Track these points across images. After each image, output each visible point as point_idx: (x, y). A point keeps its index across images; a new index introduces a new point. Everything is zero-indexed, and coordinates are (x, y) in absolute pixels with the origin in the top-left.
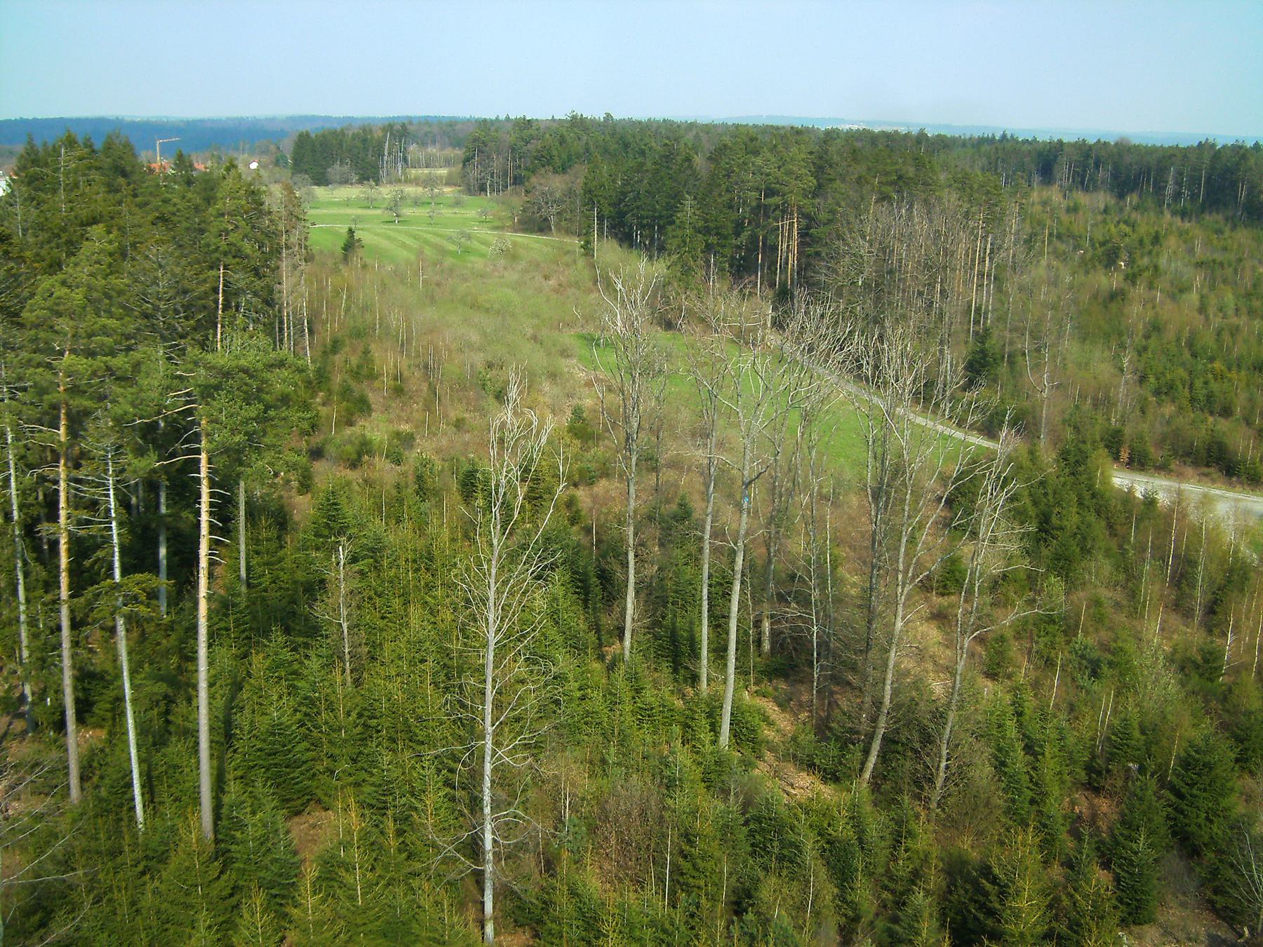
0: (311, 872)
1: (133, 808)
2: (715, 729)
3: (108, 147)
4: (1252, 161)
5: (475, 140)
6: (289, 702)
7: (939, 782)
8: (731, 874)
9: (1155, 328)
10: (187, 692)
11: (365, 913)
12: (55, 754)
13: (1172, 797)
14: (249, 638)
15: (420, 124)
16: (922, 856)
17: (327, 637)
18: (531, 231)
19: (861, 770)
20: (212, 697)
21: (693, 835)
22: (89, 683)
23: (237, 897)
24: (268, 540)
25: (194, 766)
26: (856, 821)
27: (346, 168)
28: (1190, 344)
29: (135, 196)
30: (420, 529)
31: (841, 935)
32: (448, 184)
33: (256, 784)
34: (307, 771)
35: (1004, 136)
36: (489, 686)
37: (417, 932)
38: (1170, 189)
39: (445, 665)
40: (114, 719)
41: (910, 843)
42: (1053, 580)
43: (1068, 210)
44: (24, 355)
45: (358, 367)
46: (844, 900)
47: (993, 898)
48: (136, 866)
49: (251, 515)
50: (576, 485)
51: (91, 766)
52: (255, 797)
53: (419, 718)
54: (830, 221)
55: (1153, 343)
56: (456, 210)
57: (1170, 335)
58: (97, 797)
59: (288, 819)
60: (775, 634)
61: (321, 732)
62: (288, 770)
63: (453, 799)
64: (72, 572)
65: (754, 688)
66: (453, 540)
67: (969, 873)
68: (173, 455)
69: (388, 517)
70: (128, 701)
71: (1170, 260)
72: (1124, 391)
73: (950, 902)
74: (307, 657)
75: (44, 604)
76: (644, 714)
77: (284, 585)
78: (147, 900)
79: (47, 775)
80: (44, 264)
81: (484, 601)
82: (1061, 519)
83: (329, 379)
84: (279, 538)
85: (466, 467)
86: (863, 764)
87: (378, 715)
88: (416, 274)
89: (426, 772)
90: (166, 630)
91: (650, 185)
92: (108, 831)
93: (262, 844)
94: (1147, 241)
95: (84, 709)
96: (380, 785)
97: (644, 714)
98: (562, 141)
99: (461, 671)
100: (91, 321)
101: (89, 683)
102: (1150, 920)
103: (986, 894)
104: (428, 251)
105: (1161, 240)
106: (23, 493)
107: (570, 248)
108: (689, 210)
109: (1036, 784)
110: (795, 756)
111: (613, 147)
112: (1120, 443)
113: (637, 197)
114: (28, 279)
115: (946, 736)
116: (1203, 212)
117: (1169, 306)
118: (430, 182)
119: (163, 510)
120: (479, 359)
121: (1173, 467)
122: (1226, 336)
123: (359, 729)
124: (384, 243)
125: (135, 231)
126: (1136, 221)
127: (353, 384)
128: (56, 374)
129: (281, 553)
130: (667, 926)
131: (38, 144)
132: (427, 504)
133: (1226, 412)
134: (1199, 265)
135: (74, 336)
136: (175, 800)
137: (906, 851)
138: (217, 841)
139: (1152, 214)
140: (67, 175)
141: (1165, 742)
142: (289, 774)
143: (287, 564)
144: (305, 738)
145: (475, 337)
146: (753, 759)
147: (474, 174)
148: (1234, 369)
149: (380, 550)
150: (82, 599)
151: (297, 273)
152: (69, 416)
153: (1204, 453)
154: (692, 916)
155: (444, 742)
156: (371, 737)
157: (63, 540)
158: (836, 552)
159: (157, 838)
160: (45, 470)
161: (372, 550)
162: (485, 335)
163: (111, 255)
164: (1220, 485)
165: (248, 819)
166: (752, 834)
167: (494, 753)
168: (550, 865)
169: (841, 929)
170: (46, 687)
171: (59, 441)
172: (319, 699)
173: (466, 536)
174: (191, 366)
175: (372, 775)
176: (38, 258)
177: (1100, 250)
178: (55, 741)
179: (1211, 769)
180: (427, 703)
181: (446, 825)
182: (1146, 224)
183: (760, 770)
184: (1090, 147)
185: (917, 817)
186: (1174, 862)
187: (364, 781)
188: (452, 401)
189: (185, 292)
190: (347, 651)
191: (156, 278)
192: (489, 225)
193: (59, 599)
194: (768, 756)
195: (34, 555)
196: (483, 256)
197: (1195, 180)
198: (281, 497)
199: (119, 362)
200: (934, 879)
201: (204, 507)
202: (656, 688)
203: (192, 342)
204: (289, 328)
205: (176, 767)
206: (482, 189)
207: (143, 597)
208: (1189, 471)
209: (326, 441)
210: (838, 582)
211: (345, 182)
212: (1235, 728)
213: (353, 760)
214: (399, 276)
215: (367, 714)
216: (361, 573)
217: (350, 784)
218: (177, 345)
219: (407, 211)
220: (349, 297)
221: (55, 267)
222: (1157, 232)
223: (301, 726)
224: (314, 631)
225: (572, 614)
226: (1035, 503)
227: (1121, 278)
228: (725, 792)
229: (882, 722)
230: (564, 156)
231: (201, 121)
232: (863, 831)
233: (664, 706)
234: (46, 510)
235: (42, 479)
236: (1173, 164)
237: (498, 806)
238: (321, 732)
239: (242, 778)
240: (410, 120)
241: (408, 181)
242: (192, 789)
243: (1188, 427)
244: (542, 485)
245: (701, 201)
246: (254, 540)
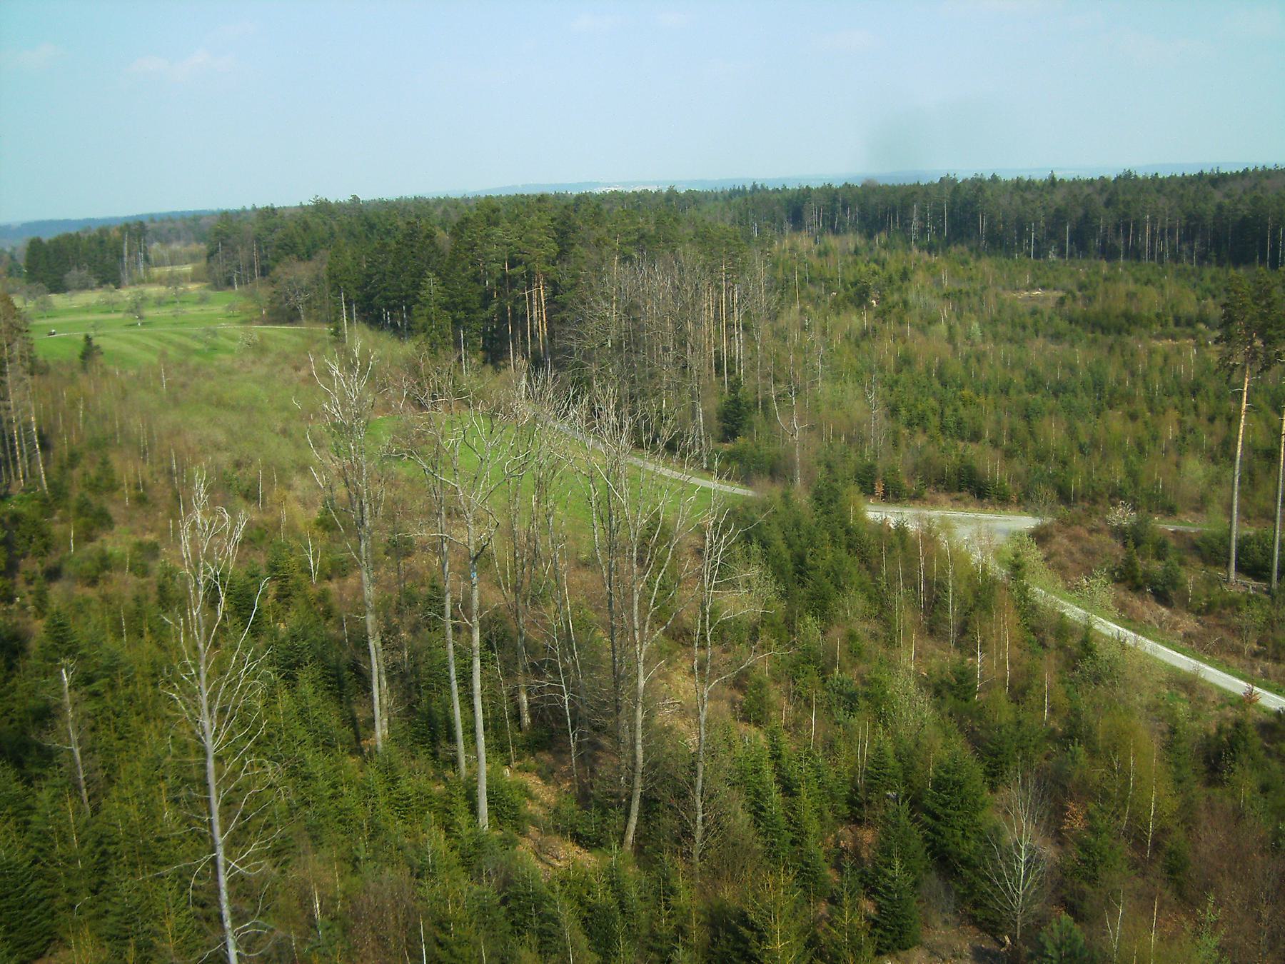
2: (473, 809)
4: (989, 193)
7: (698, 835)
9: (905, 362)
13: (929, 820)
18: (281, 322)
27: (84, 273)
28: (940, 375)
32: (194, 280)
34: (46, 910)
35: (754, 187)
36: (213, 796)
38: (915, 225)
42: (809, 619)
43: (820, 254)
50: (329, 578)
54: (574, 286)
55: (903, 377)
57: (920, 367)
61: (58, 866)
62: (23, 912)
65: (515, 764)
67: (728, 923)
71: (918, 293)
72: (876, 423)
73: (714, 953)
82: (814, 559)
83: (67, 496)
91: (394, 265)
94: (896, 277)
96: (122, 914)
98: (306, 227)
102: (916, 943)
103: (746, 941)
104: (171, 352)
105: (910, 275)
107: (319, 336)
108: (432, 284)
109: (795, 825)
111: (358, 229)
112: (873, 478)
113: (381, 281)
115: (699, 789)
116: (948, 245)
117: (920, 338)
118: (173, 280)
120: (224, 458)
121: (926, 495)
122: (973, 362)
124: (126, 348)
126: (885, 259)
133: (976, 437)
134: (946, 296)
139: (900, 251)
141: (920, 767)
142: (24, 915)
144: (40, 875)
145: (221, 437)
147: (218, 270)
148: (982, 394)
153: (954, 478)
162: (230, 432)
164: (973, 508)
177: (852, 291)
179: (961, 787)
182: (894, 262)
183: (525, 848)
184: (836, 191)
186: (933, 881)
187: (107, 912)
190: (82, 777)
192: (238, 319)
194: (532, 830)
196: (231, 351)
197: (938, 214)
200: (697, 934)
206: (229, 283)
208: (943, 497)
209: (62, 560)
211: (85, 287)
212: (988, 744)
220: (86, 407)
222: (905, 268)
224: (47, 756)
226: (790, 546)
227: (871, 316)
229: (638, 782)
230: (308, 242)
232: (623, 895)
236: (914, 201)
238: (58, 866)
240: (152, 218)
241: (152, 281)
243: (938, 455)
244: (291, 582)
245: (444, 280)
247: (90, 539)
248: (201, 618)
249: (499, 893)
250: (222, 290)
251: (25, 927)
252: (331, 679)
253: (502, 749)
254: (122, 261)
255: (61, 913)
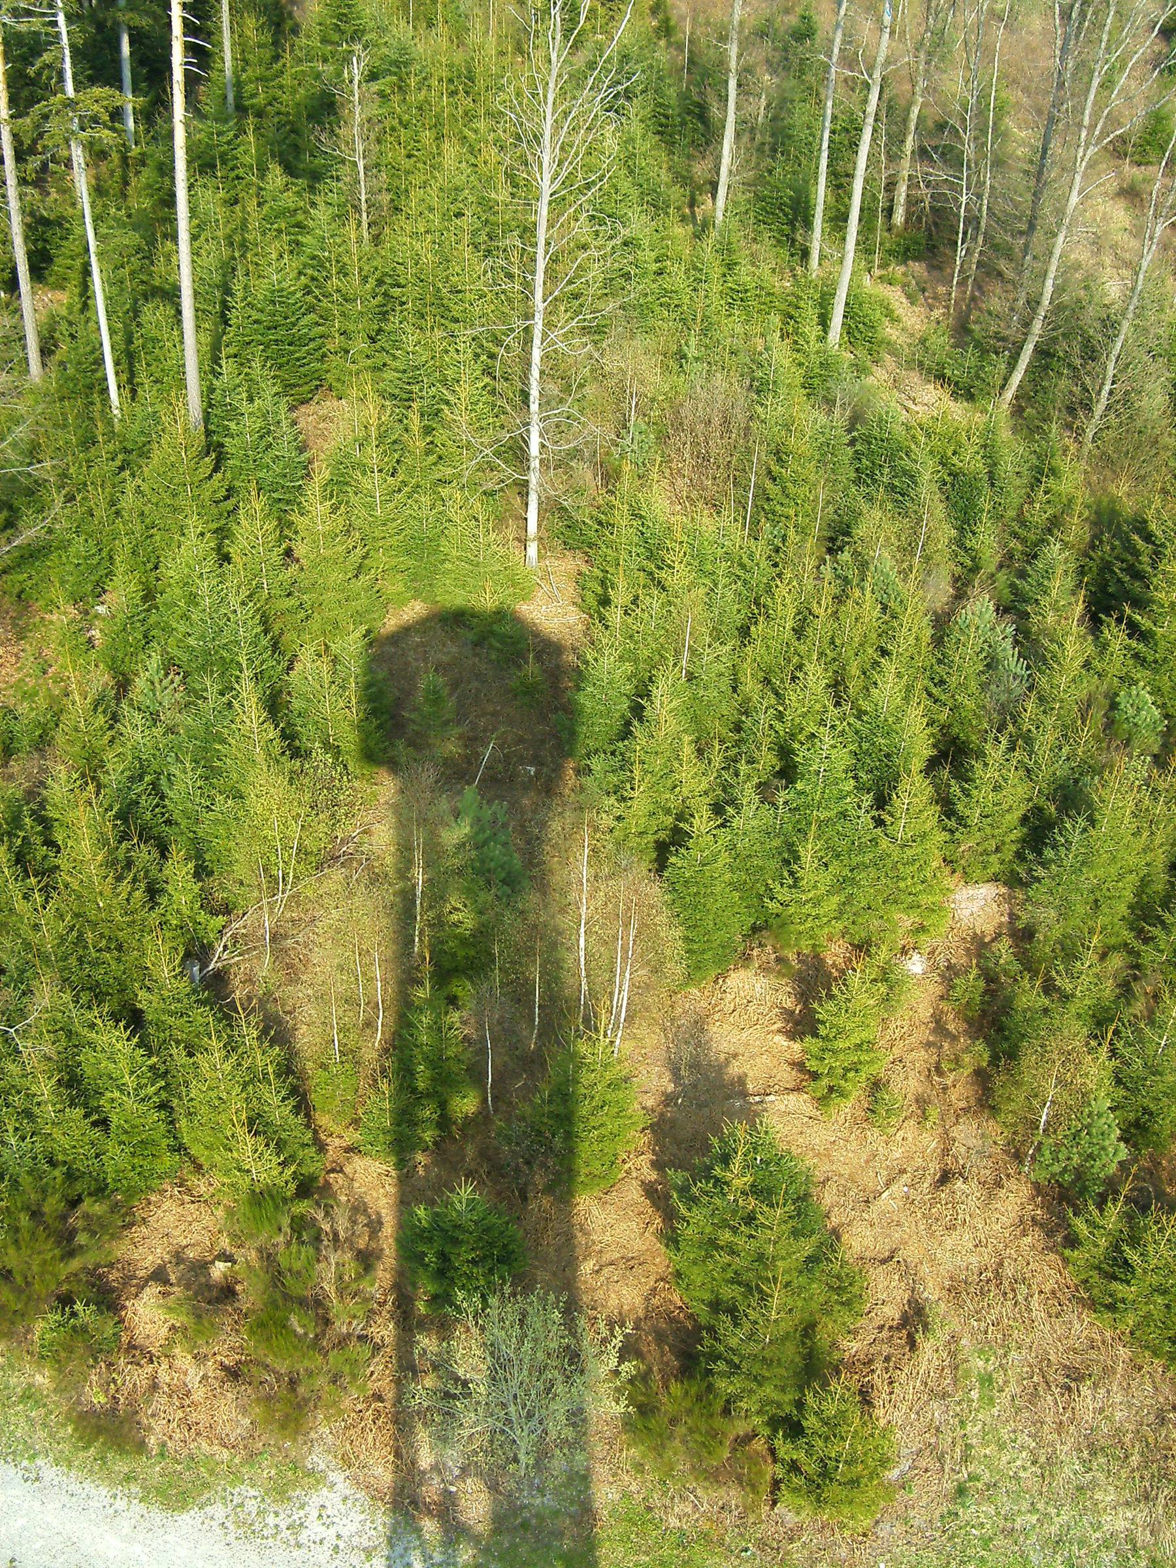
0: (322, 473)
1: (105, 391)
2: (824, 321)
6: (292, 264)
7: (1099, 409)
8: (829, 502)
11: (385, 525)
16: (1064, 500)
19: (1003, 387)
21: (785, 453)
23: (233, 501)
25: (177, 339)
26: (989, 451)
30: (459, 37)
31: (954, 587)
33: (253, 364)
37: (446, 550)
39: (487, 221)
41: (1052, 483)
46: (961, 545)
47: (1145, 559)
48: (113, 460)
51: (52, 337)
59: (292, 409)
60: (911, 202)
63: (493, 392)
65: (877, 272)
66: (502, 54)
69: (416, 18)
76: (737, 297)
77: (283, 109)
78: (128, 501)
86: (1006, 380)
89: (461, 357)
93: (261, 437)
95: (40, 264)
96: (405, 371)
97: (737, 297)
103: (1136, 553)
110: (921, 364)
115: (1115, 352)
129: (277, 66)
130: (745, 560)
137: (1046, 493)
138: (208, 433)
142: (292, 353)
144: (311, 309)
146: (869, 363)
149: (406, 64)
154: (777, 550)
158: (1003, 95)
159: (136, 427)
161: (396, 63)
165: (245, 407)
166: (858, 456)
167: (545, 335)
168: (609, 476)
169: (956, 579)
173: (519, 50)
175: (395, 358)
181: (484, 423)
183: (878, 377)
185: (1065, 450)
200: (1077, 530)
202: (753, 264)
205: (155, 340)
210: (1001, 135)
213: (370, 337)
216: (382, 94)
223: (308, 293)
225: (652, 162)
228: (830, 402)
229: (1037, 327)
233: (762, 288)
237: (548, 403)
239: (235, 356)
249: (849, 431)
252: (663, 120)
253: (869, 251)
255: (332, 357)
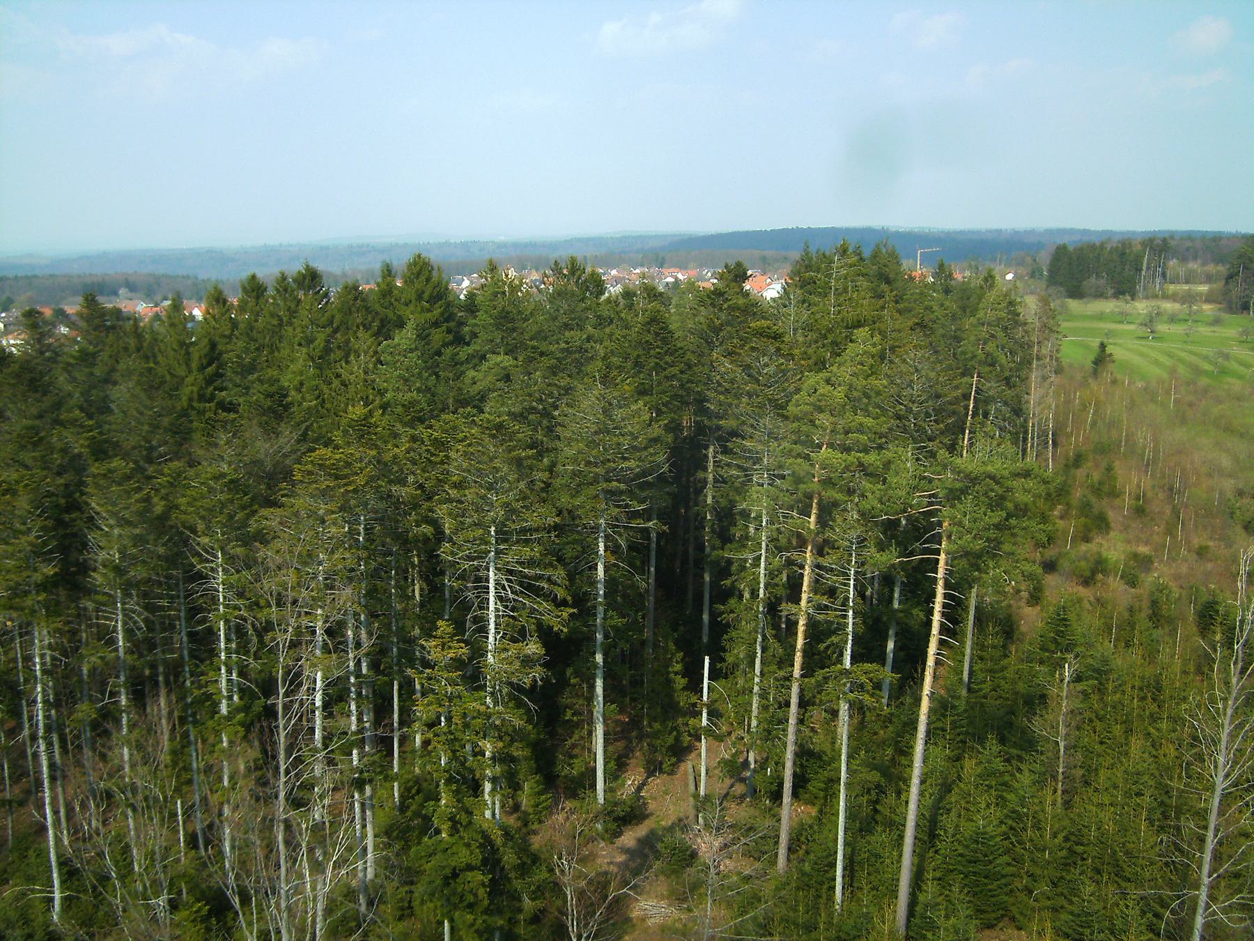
3: (876, 255)
5: (1240, 257)
10: (897, 785)
12: (768, 822)
14: (964, 742)
15: (1182, 239)
17: (1042, 753)
20: (921, 794)
22: (807, 761)
24: (994, 647)
27: (1102, 282)
29: (897, 302)
30: (1151, 655)
32: (1208, 301)
40: (826, 799)
44: (786, 444)
45: (1100, 483)
49: (979, 619)
51: (799, 840)
52: (949, 901)
53: (1127, 853)
56: (1215, 329)
58: (801, 870)
61: (1025, 849)
62: (986, 881)
64: (808, 652)
66: (1185, 672)
68: (912, 554)
69: (1117, 640)
70: (842, 784)
74: (1020, 770)
75: (776, 679)
79: (760, 840)
80: (810, 362)
81: (1215, 742)
83: (1068, 493)
84: (1004, 646)
85: (1205, 598)
87: (1086, 842)
88: (1168, 393)
90: (884, 722)
92: (807, 905)
95: (800, 782)
96: (1079, 915)
99: (1179, 812)
100: (850, 419)
101: (807, 761)
104: (1182, 370)
106: (771, 574)
114: (795, 375)
118: (1188, 299)
119: (896, 605)
120: (1229, 485)
123: (1064, 853)
124: (1136, 360)
125: (894, 335)
127: (1093, 500)
128: (812, 465)
129: (1005, 662)
131: (812, 250)
132: (1160, 631)
135: (832, 431)
136: (873, 889)
140: (837, 280)
143: (1010, 674)
144: (1007, 852)
145: (1226, 462)
147: (1236, 291)
149: (1106, 673)
150: (813, 680)
151: (1046, 384)
152: (821, 508)
155: (1152, 883)
156: (1075, 863)
157: (802, 622)
159: (851, 922)
160: (794, 555)
161: (1098, 671)
162: (1237, 460)
163: (873, 357)
165: (941, 922)
167: (1208, 906)
170: (767, 759)
171: (809, 528)
172: (1027, 815)
173: (1199, 671)
174: (939, 469)
175: (1071, 903)
176: (806, 356)
178: (770, 810)
180: (1139, 839)
187: (1062, 907)
188: (1196, 527)
189: (938, 396)
191: (912, 381)
193: (792, 676)
195: (774, 632)
196: (1241, 377)
198: (1010, 606)
199: (872, 458)
201: (938, 607)
203: (940, 445)
204: (1033, 439)
205: (878, 856)
207: (869, 687)
211: (1100, 295)
213: (1053, 883)
214: (1150, 394)
215: (1074, 839)
217: (1048, 908)
218: (925, 447)
219: (1162, 328)
220: (1095, 412)
221: (820, 365)
223: (1005, 839)
224: (1029, 744)
231: (961, 232)
234: (788, 592)
235: (790, 562)
238: (1025, 849)
239: (940, 879)
240: (1172, 235)
241: (1165, 297)
242: (890, 881)
246: (979, 645)
247: (1087, 540)
248: (1240, 652)
250: (1235, 313)
251: (986, 895)
254: (1140, 275)
